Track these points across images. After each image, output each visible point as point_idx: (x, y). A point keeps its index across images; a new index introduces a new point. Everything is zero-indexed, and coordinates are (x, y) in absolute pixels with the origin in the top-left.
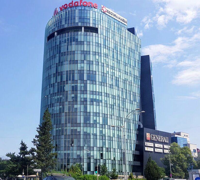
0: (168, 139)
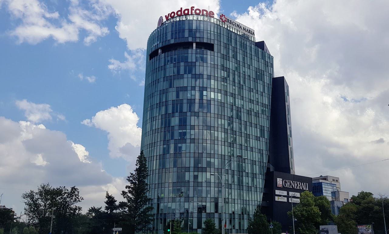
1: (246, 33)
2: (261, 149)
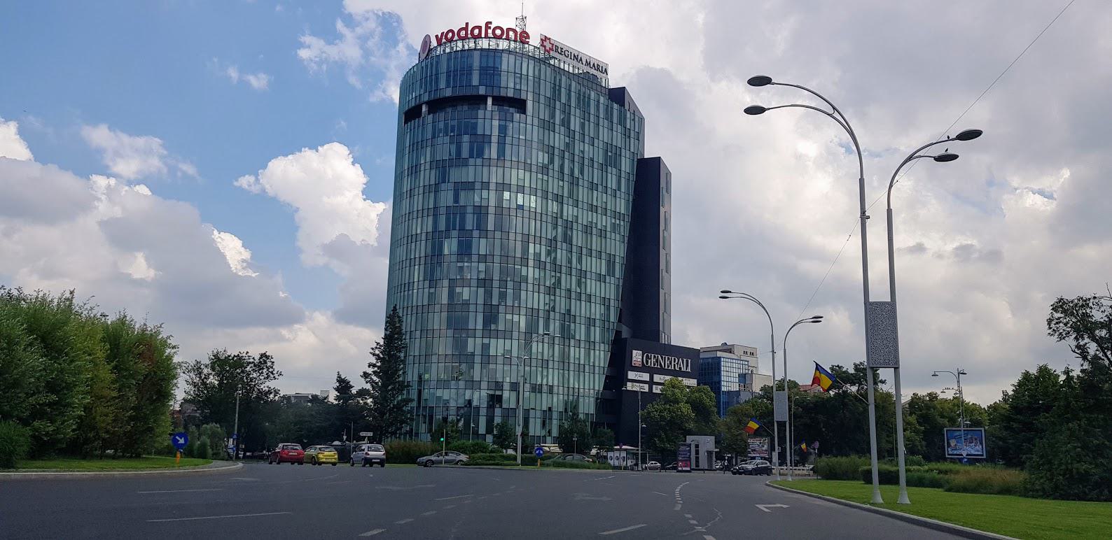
0: (689, 365)
1: (595, 72)
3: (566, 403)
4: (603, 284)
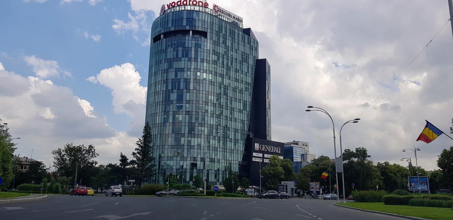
1: (236, 21)
2: (244, 119)
3: (226, 167)
4: (241, 114)
